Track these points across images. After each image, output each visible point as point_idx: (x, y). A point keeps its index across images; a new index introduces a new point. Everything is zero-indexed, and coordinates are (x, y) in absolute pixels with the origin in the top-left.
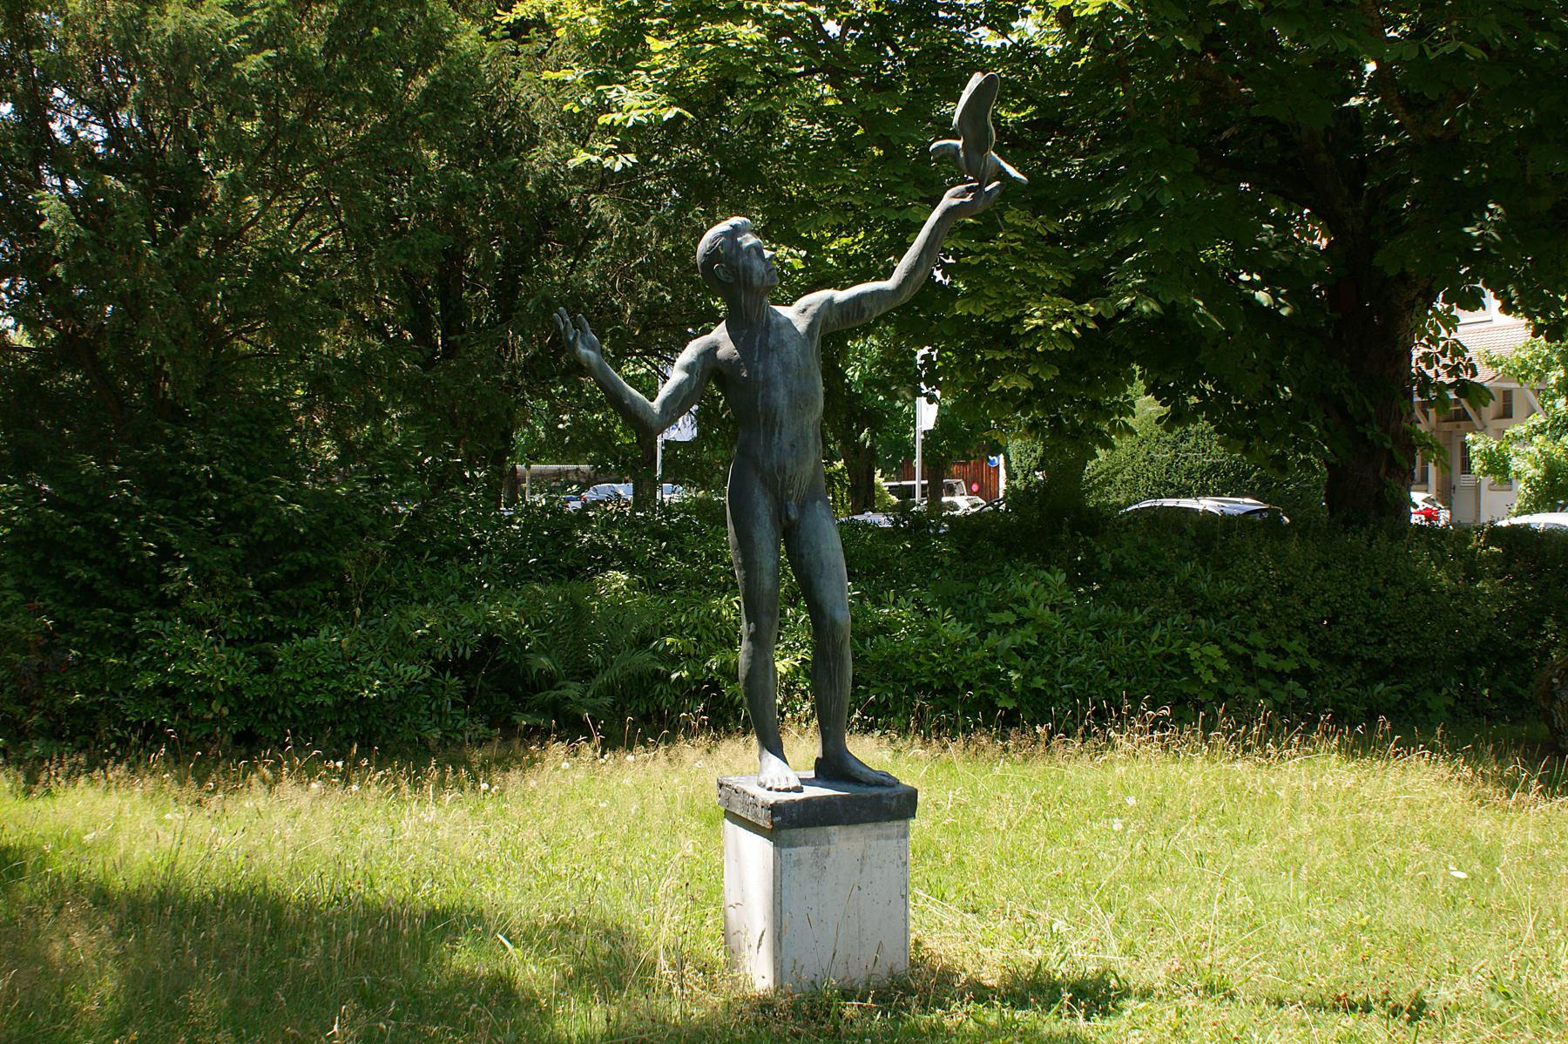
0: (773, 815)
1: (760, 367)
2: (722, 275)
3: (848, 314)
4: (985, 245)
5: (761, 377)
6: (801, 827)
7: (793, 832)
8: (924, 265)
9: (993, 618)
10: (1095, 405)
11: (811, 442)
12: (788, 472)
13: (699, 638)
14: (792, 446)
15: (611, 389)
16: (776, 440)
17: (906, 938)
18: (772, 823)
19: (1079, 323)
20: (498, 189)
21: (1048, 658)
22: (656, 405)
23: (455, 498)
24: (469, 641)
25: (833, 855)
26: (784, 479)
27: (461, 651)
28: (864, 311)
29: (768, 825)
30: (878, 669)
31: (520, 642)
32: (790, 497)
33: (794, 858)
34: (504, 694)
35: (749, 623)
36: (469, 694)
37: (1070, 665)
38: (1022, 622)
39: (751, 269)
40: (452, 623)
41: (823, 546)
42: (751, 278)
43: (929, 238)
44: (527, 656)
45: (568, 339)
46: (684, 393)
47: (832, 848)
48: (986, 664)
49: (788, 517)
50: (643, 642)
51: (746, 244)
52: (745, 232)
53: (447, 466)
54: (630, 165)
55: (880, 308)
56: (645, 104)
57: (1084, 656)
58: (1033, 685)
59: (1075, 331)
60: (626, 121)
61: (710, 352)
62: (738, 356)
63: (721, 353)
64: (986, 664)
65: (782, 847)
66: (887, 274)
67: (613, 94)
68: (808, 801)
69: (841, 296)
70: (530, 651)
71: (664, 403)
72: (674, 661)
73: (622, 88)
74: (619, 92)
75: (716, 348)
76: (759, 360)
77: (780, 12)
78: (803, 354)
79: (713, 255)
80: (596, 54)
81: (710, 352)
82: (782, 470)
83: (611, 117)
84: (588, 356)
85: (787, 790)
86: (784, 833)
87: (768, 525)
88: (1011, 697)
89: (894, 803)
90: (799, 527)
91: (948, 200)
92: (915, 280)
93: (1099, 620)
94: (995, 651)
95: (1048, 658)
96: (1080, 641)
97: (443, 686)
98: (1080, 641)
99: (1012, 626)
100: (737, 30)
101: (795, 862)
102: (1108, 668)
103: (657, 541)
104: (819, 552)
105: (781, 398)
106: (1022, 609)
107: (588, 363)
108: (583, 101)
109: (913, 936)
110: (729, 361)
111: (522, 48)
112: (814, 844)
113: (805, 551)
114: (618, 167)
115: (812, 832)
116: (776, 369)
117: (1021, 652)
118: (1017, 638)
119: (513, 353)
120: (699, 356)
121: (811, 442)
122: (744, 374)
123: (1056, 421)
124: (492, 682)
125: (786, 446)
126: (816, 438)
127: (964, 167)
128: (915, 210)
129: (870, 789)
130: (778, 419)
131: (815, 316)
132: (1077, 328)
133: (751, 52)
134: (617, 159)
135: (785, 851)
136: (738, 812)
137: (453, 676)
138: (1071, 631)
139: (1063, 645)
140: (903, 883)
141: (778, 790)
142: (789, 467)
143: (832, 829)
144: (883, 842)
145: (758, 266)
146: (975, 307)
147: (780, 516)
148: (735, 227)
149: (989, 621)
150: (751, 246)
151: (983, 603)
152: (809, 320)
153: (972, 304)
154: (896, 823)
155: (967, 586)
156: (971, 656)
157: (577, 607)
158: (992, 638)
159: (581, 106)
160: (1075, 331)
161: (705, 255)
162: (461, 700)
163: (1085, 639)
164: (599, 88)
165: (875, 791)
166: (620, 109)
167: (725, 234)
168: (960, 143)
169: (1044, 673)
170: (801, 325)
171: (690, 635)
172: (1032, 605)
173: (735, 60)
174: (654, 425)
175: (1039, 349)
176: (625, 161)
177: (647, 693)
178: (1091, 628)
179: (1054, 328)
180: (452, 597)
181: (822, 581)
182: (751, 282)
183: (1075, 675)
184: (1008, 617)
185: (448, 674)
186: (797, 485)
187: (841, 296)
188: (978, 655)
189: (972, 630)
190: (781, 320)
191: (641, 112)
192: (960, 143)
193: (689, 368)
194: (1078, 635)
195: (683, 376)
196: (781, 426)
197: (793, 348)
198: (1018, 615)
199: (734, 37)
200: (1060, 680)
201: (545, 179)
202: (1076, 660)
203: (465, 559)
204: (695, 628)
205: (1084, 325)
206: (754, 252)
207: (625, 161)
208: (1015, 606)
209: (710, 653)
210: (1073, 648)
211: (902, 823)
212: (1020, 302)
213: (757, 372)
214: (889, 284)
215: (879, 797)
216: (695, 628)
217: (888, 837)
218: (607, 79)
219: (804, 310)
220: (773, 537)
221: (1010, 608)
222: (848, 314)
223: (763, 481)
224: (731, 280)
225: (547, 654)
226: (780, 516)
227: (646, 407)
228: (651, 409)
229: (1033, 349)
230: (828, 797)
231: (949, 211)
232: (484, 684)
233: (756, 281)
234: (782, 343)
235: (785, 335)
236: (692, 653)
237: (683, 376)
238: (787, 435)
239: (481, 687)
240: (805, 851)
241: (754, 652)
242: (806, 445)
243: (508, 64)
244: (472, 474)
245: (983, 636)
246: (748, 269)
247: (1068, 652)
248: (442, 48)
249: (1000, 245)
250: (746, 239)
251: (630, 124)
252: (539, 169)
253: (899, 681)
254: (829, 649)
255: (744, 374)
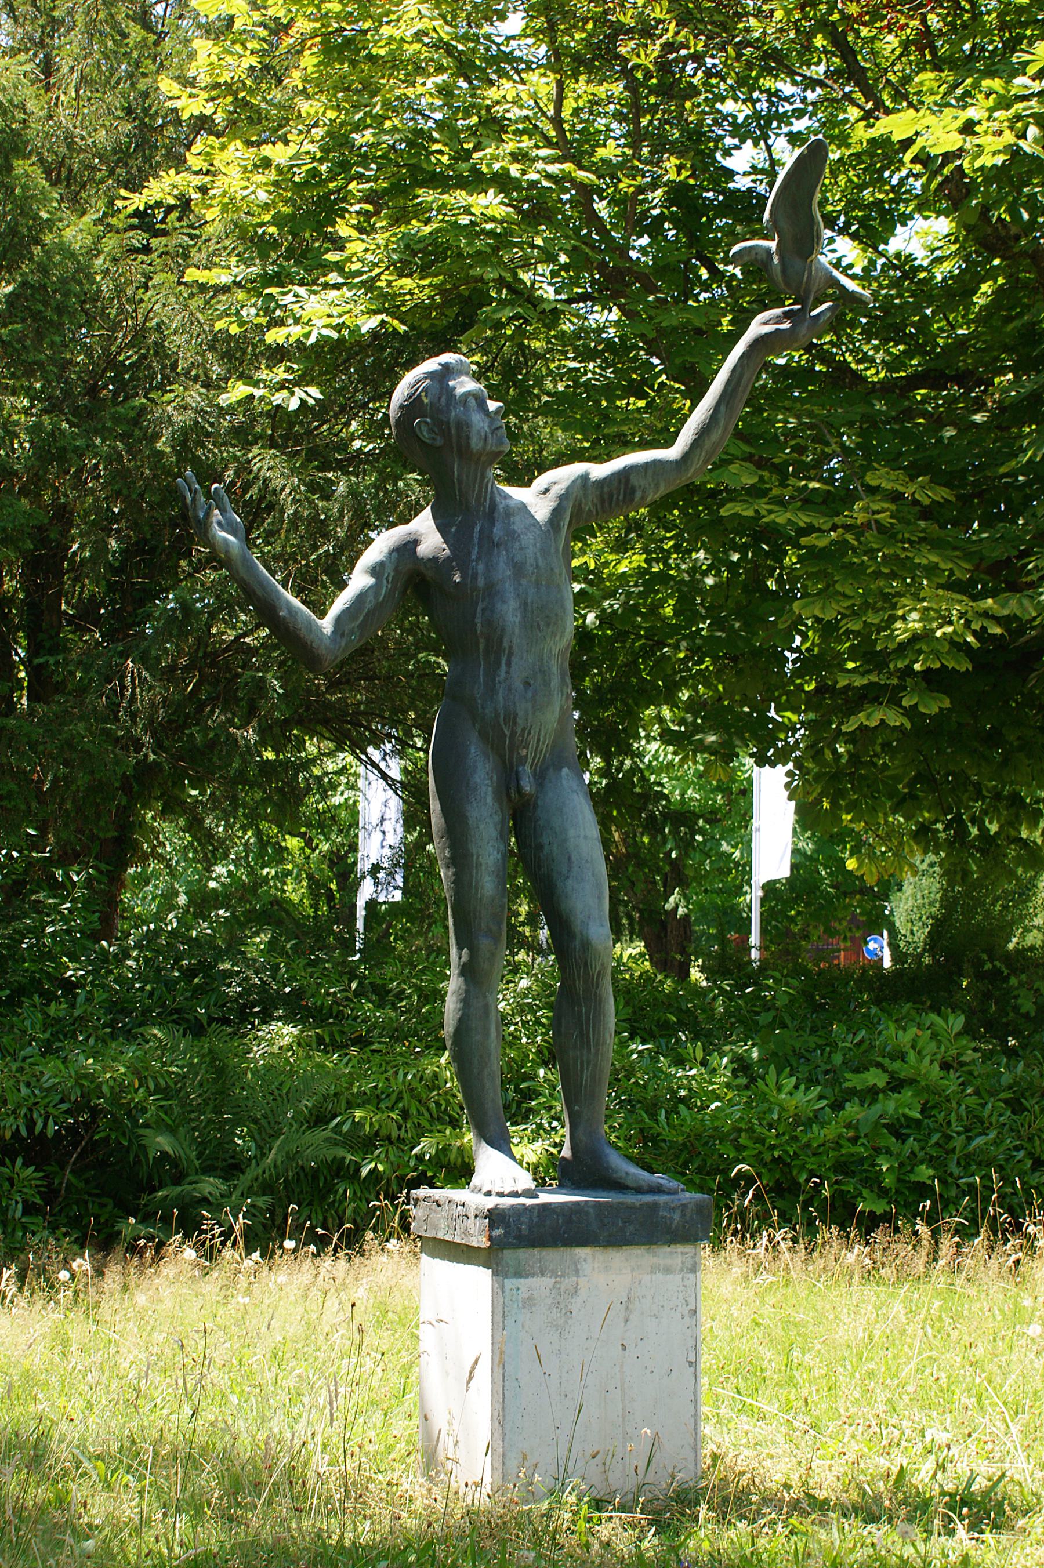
0: (491, 1227)
1: (481, 567)
2: (425, 435)
3: (611, 495)
4: (837, 520)
5: (481, 582)
6: (534, 1246)
7: (523, 1254)
8: (722, 423)
9: (853, 1081)
10: (1015, 800)
11: (555, 682)
12: (520, 721)
13: (405, 1114)
14: (527, 684)
15: (259, 593)
16: (503, 674)
17: (695, 1449)
18: (490, 1238)
19: (976, 626)
20: (115, 448)
21: (936, 1137)
22: (327, 624)
23: (38, 907)
24: (51, 1110)
25: (583, 1292)
26: (513, 734)
27: (39, 1125)
28: (633, 491)
29: (484, 1243)
30: (677, 1157)
31: (134, 1111)
32: (522, 761)
33: (524, 1294)
34: (105, 1200)
35: (460, 948)
36: (50, 1194)
37: (971, 1148)
38: (896, 1085)
39: (468, 425)
40: (28, 1085)
41: (571, 833)
42: (468, 438)
43: (728, 382)
44: (141, 1131)
45: (197, 516)
46: (368, 606)
47: (582, 1281)
48: (841, 1146)
49: (519, 790)
50: (319, 1119)
51: (460, 391)
52: (461, 373)
53: (31, 863)
54: (311, 402)
55: (657, 486)
56: (335, 311)
57: (992, 1135)
58: (913, 1178)
59: (970, 639)
60: (307, 335)
61: (407, 548)
62: (447, 551)
63: (423, 550)
64: (841, 1146)
65: (506, 1276)
66: (669, 443)
67: (289, 298)
68: (545, 1207)
69: (599, 471)
70: (146, 1126)
71: (338, 620)
72: (367, 1144)
73: (302, 291)
74: (296, 296)
75: (416, 542)
76: (479, 558)
77: (534, 177)
78: (545, 552)
79: (413, 406)
80: (262, 246)
81: (407, 548)
82: (511, 718)
83: (283, 331)
84: (225, 540)
85: (515, 1194)
86: (508, 1255)
87: (489, 800)
88: (879, 1197)
89: (677, 1216)
90: (536, 806)
91: (757, 328)
92: (708, 444)
93: (1016, 1083)
94: (856, 1129)
95: (936, 1137)
96: (987, 1112)
97: (11, 1181)
98: (987, 1112)
99: (883, 1091)
100: (471, 200)
101: (524, 1301)
102: (1030, 1155)
103: (345, 978)
104: (565, 840)
105: (510, 612)
106: (897, 1065)
107: (227, 552)
108: (244, 313)
109: (709, 1448)
110: (435, 559)
111: (154, 242)
112: (554, 1274)
113: (545, 840)
114: (294, 404)
115: (552, 1256)
116: (503, 570)
117: (898, 1129)
118: (890, 1106)
119: (133, 694)
120: (391, 552)
121: (555, 682)
122: (457, 578)
123: (958, 825)
124: (87, 1182)
125: (518, 684)
126: (563, 679)
127: (782, 285)
128: (710, 360)
129: (640, 1197)
130: (505, 644)
131: (562, 498)
132: (974, 633)
133: (491, 234)
134: (292, 394)
135: (510, 1283)
136: (440, 1236)
137: (26, 1165)
138: (972, 1101)
139: (959, 1118)
140: (691, 1342)
141: (501, 1195)
142: (521, 714)
143: (583, 1253)
144: (659, 1277)
145: (478, 421)
146: (823, 608)
147: (508, 789)
148: (446, 367)
149: (847, 1085)
150: (468, 394)
151: (838, 1059)
152: (553, 504)
153: (819, 605)
154: (680, 1248)
155: (813, 1041)
156: (820, 1134)
157: (221, 1072)
158: (852, 1109)
159: (241, 323)
160: (970, 639)
161: (402, 407)
162: (38, 1200)
163: (993, 1109)
164: (267, 291)
165: (649, 1198)
166: (297, 321)
167: (431, 375)
168: (773, 245)
169: (931, 1161)
170: (541, 509)
171: (392, 1109)
172: (912, 1056)
173: (468, 244)
174: (322, 651)
175: (917, 667)
176: (304, 396)
177: (324, 1198)
178: (1002, 1096)
179: (938, 634)
180: (28, 1051)
181: (570, 883)
182: (468, 445)
183: (979, 1164)
184: (875, 1078)
185: (19, 1162)
186: (533, 744)
187: (599, 471)
188: (830, 1132)
189: (821, 1097)
190: (511, 503)
191: (329, 320)
192: (773, 245)
193: (376, 571)
194: (983, 1106)
195: (369, 581)
196: (510, 654)
197: (529, 540)
198: (892, 1075)
199: (467, 210)
200: (956, 1171)
201: (185, 431)
202: (980, 1141)
203: (49, 998)
204: (400, 1098)
205: (984, 629)
206: (472, 402)
207: (304, 396)
208: (886, 1062)
209: (420, 1132)
210: (976, 1124)
211: (688, 1249)
212: (889, 601)
213: (475, 576)
214: (672, 453)
215: (654, 1207)
216: (400, 1098)
217: (668, 1270)
218: (279, 279)
219: (546, 491)
220: (497, 818)
221: (879, 1065)
222: (611, 495)
223: (483, 735)
224: (439, 442)
225: (172, 1131)
226: (508, 789)
227: (310, 623)
228: (319, 629)
229: (909, 669)
230: (578, 1203)
231: (761, 343)
232: (73, 1180)
233: (476, 444)
234: (512, 536)
235: (518, 524)
236: (394, 1134)
237: (369, 581)
238: (519, 668)
239: (69, 1185)
240: (539, 1285)
241: (467, 992)
242: (547, 684)
243: (135, 266)
244: (66, 875)
245: (837, 1106)
246: (463, 426)
247: (967, 1130)
248: (37, 242)
249: (861, 518)
250: (462, 383)
251: (312, 340)
252: (178, 418)
253: (708, 1174)
254: (580, 984)
255: (457, 578)
